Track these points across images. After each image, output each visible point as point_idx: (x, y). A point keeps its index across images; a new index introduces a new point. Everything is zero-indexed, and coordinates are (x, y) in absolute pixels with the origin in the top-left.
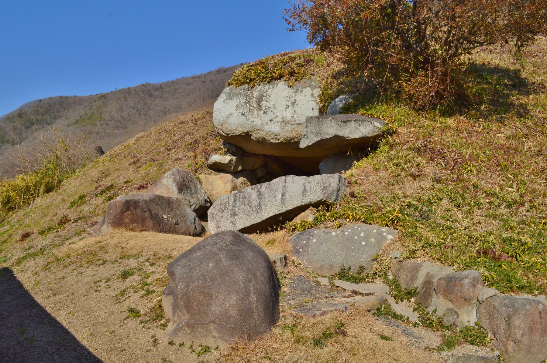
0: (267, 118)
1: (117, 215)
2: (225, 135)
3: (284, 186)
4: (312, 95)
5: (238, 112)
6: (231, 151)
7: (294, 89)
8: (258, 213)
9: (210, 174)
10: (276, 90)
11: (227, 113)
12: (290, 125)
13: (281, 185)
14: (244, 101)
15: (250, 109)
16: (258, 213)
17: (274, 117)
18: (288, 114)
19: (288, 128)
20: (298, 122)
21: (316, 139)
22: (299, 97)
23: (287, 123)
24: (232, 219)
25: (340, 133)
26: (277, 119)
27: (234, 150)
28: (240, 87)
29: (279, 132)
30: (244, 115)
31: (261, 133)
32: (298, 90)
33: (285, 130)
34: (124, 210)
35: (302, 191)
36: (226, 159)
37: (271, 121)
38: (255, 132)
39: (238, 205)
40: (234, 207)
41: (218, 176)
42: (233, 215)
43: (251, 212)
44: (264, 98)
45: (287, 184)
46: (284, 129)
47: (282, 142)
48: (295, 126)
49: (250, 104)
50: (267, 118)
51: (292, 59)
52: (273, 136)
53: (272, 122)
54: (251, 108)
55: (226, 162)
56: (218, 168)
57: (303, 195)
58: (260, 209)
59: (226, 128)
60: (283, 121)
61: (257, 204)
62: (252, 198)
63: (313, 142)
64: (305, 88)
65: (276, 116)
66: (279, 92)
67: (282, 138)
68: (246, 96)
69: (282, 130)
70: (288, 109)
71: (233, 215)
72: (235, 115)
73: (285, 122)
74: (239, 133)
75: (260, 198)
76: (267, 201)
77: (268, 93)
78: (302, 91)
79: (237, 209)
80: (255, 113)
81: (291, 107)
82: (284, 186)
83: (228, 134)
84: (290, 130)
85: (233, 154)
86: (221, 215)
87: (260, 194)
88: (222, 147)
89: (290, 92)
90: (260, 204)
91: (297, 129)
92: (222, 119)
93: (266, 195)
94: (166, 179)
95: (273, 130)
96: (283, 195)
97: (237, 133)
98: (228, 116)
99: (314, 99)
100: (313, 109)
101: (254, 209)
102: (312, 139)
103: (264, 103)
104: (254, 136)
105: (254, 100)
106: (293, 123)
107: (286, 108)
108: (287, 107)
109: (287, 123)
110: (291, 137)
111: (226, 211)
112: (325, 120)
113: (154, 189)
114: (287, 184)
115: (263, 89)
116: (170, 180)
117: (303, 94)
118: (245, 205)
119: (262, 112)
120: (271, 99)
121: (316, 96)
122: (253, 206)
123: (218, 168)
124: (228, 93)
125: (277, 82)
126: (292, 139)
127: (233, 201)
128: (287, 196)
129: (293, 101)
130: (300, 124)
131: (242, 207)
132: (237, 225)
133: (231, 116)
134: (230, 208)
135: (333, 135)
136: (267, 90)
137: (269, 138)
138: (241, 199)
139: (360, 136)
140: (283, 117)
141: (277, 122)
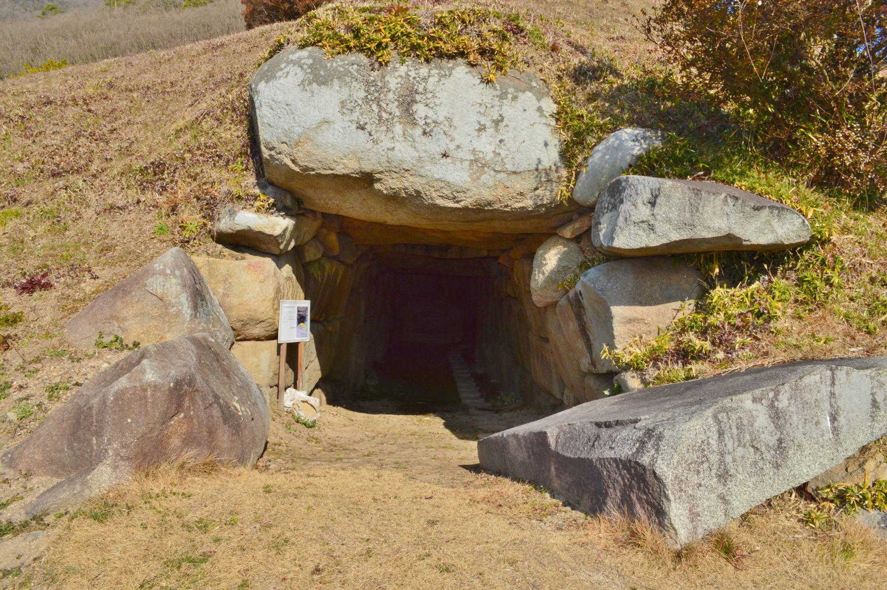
0: (434, 146)
1: (152, 430)
2: (297, 169)
3: (832, 395)
4: (540, 109)
5: (347, 118)
6: (279, 205)
7: (495, 89)
8: (777, 466)
9: (220, 255)
10: (449, 83)
11: (317, 117)
12: (492, 173)
13: (825, 390)
14: (362, 94)
15: (380, 117)
16: (777, 466)
17: (452, 146)
18: (486, 145)
19: (487, 178)
20: (510, 168)
21: (675, 237)
22: (510, 111)
23: (484, 166)
24: (721, 489)
25: (738, 232)
26: (461, 154)
27: (289, 202)
28: (342, 56)
29: (466, 186)
30: (363, 128)
31: (411, 179)
32: (506, 93)
33: (481, 182)
34: (173, 410)
35: (868, 406)
36: (278, 224)
37: (445, 155)
38: (394, 175)
39: (730, 446)
40: (722, 454)
41: (244, 263)
42: (724, 476)
43: (760, 464)
44: (418, 97)
45: (837, 390)
46: (478, 178)
47: (466, 209)
48: (503, 175)
49: (379, 106)
50: (434, 146)
51: (482, 18)
52: (446, 192)
53: (449, 160)
54: (385, 116)
55: (277, 232)
56: (243, 242)
57: (873, 418)
58: (785, 458)
59: (309, 154)
60: (476, 161)
61: (773, 441)
62: (756, 425)
63: (664, 241)
64: (524, 91)
65: (458, 147)
66: (456, 90)
67: (470, 200)
68: (368, 83)
69: (474, 180)
70: (484, 134)
71: (724, 476)
72: (338, 126)
73: (478, 164)
74: (346, 172)
75: (778, 427)
76: (799, 435)
77: (430, 87)
78: (515, 98)
79: (728, 459)
80: (398, 129)
81: (490, 131)
82: (832, 395)
83: (306, 169)
84: (491, 183)
85: (287, 211)
86: (695, 479)
87: (776, 415)
88: (257, 191)
89: (487, 94)
90: (780, 441)
91: (508, 184)
92: (298, 130)
93: (795, 418)
94: (161, 279)
95: (450, 178)
96: (834, 419)
97: (340, 170)
98: (319, 126)
99: (544, 120)
100: (546, 145)
101: (768, 456)
102: (664, 235)
103: (420, 110)
104: (388, 184)
105: (391, 96)
106: (498, 168)
107: (479, 130)
108: (482, 129)
109: (484, 166)
110: (491, 198)
111: (706, 465)
112: (712, 197)
113: (119, 304)
114: (837, 390)
115: (412, 74)
116: (174, 281)
117: (519, 105)
118: (744, 446)
119: (418, 131)
120: (438, 101)
121: (547, 114)
122: (763, 449)
123: (243, 242)
124: (310, 66)
125: (449, 64)
126: (490, 204)
127: (716, 437)
128: (842, 420)
129: (496, 116)
130: (515, 173)
131: (740, 451)
132: (736, 504)
133: (325, 126)
134: (714, 458)
135: (723, 234)
136: (425, 79)
137: (434, 195)
138: (735, 431)
139: (770, 242)
140: (474, 151)
141: (462, 161)
